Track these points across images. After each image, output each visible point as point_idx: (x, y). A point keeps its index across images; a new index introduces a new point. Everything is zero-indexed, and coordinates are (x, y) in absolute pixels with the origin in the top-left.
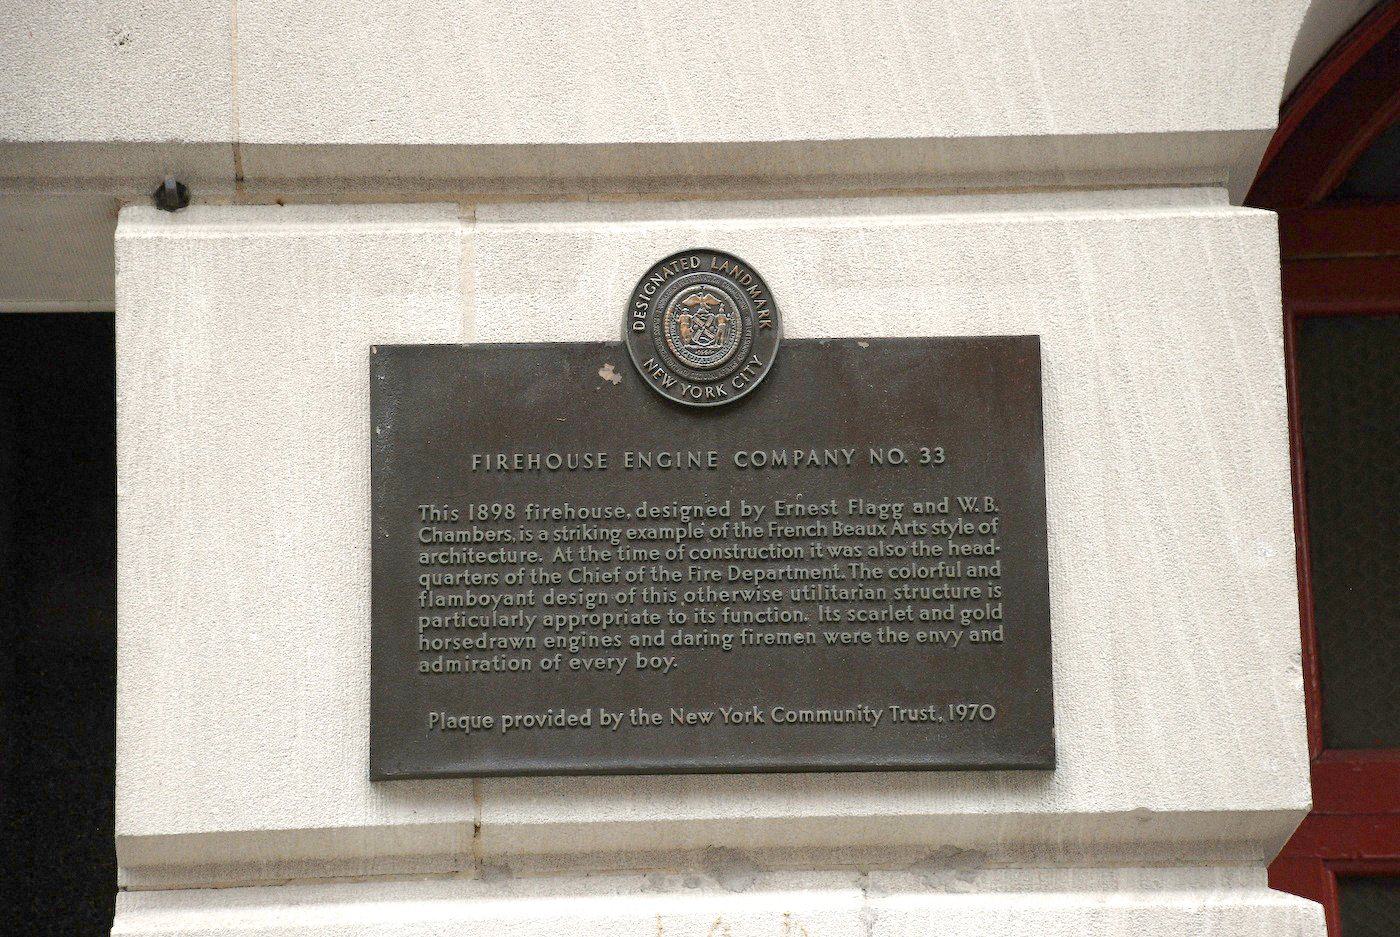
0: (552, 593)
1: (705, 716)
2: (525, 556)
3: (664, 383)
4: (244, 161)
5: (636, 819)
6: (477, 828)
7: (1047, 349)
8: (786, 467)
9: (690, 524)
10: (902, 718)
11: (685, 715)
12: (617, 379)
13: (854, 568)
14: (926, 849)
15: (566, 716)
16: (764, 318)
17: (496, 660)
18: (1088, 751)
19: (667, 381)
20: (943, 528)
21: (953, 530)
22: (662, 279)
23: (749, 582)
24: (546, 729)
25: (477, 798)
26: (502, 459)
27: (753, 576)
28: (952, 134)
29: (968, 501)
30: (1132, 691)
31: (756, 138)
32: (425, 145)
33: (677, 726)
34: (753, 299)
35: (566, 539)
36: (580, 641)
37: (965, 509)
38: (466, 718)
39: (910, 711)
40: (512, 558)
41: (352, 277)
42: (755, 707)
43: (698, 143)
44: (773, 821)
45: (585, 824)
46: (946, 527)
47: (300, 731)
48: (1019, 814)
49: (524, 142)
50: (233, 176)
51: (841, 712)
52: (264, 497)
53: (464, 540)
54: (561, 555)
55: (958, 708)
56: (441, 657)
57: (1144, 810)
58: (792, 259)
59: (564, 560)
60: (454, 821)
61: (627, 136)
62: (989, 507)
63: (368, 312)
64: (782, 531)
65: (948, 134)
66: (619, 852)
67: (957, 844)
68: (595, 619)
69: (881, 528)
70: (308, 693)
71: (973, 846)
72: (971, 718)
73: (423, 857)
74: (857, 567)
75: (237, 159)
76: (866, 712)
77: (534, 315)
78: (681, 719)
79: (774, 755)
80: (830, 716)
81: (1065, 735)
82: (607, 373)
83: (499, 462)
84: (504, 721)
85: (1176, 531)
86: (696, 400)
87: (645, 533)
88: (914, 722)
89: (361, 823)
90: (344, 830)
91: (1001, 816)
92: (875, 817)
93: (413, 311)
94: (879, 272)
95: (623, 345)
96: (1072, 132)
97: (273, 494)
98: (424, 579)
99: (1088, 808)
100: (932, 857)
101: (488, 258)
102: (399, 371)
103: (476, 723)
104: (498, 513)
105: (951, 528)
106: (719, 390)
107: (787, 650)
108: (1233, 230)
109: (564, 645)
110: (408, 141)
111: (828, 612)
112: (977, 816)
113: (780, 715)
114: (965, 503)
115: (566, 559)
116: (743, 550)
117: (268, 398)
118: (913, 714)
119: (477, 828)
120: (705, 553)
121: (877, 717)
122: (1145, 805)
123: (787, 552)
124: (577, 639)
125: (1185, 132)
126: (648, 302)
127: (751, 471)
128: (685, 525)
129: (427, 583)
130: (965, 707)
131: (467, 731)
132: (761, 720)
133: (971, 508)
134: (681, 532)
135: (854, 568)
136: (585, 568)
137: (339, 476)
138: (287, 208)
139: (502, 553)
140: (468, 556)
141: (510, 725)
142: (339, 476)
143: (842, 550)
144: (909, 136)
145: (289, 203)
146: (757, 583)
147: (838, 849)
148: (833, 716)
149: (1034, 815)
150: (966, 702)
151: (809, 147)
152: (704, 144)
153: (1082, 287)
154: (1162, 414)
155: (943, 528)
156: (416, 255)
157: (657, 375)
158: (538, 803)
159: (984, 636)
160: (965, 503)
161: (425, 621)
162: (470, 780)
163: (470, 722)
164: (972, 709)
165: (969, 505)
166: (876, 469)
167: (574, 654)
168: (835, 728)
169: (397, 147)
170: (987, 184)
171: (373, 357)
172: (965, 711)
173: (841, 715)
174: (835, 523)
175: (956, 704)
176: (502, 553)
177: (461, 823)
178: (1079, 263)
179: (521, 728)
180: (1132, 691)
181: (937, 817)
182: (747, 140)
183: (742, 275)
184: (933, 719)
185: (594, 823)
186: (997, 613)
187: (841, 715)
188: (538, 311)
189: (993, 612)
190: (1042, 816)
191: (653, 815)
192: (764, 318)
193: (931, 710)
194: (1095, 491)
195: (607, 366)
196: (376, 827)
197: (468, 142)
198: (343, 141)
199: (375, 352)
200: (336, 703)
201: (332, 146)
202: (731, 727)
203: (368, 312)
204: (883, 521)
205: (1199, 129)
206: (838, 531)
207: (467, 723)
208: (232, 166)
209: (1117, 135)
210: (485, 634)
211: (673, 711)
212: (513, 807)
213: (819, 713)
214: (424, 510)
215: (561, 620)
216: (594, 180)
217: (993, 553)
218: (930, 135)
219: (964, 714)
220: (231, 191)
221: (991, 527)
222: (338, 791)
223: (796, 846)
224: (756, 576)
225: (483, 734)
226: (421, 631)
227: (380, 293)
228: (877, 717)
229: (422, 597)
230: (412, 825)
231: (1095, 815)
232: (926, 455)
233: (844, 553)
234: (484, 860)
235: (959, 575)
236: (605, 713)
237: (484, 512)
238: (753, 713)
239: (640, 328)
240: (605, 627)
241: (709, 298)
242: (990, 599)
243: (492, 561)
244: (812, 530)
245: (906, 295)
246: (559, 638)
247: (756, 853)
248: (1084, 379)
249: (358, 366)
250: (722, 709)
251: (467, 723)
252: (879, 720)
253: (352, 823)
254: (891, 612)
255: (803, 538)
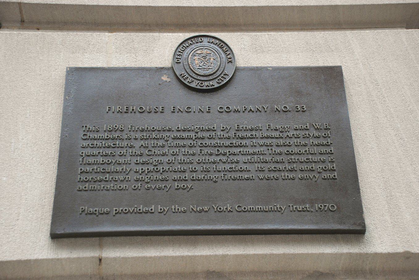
0: (139, 159)
1: (206, 209)
2: (127, 144)
3: (188, 80)
4: (24, 12)
5: (174, 255)
6: (100, 260)
7: (343, 68)
8: (239, 112)
9: (199, 133)
10: (295, 209)
11: (197, 208)
12: (169, 80)
13: (270, 149)
14: (307, 273)
15: (143, 208)
16: (229, 58)
17: (112, 185)
18: (379, 226)
19: (190, 79)
20: (307, 134)
21: (312, 136)
22: (187, 45)
23: (225, 154)
24: (133, 214)
25: (101, 246)
26: (119, 108)
27: (226, 153)
28: (300, 5)
29: (317, 125)
30: (396, 202)
31: (225, 5)
32: (96, 5)
33: (193, 213)
34: (225, 52)
35: (146, 138)
36: (150, 177)
37: (316, 127)
38: (97, 209)
39: (298, 207)
40: (122, 145)
41: (62, 47)
42: (228, 205)
43: (202, 7)
44: (237, 256)
45: (151, 258)
46: (309, 134)
47: (21, 217)
48: (350, 253)
49: (135, 5)
50: (20, 20)
51: (267, 207)
52: (16, 124)
53: (101, 138)
54: (143, 144)
55: (319, 206)
56: (87, 184)
57: (408, 252)
58: (240, 44)
59: (144, 146)
60: (90, 256)
61: (174, 4)
62: (326, 127)
63: (68, 59)
64: (238, 135)
65: (298, 4)
66: (166, 274)
67: (321, 270)
68: (157, 169)
69: (281, 135)
70: (26, 202)
71: (328, 271)
72: (326, 209)
73: (75, 276)
74: (271, 149)
75: (21, 12)
76: (278, 207)
77: (136, 61)
78: (195, 210)
79: (238, 225)
80: (262, 208)
81: (369, 221)
82: (165, 78)
83: (118, 109)
84: (114, 210)
85: (406, 139)
86: (202, 86)
87: (180, 136)
88: (300, 211)
89: (45, 257)
90: (36, 261)
91: (342, 254)
92: (284, 254)
93: (87, 59)
94: (275, 48)
95: (172, 68)
96: (346, 4)
97: (20, 123)
98: (82, 153)
99: (382, 251)
100: (309, 276)
101: (119, 42)
102: (76, 74)
103: (101, 211)
104: (117, 128)
105: (311, 134)
106: (211, 83)
107: (242, 182)
108: (414, 34)
109: (143, 179)
110: (89, 4)
111: (259, 166)
112: (331, 254)
113: (239, 208)
114: (316, 125)
115: (145, 145)
116: (222, 143)
117: (22, 88)
118: (300, 208)
119: (100, 260)
120: (206, 144)
121: (283, 209)
122: (408, 250)
123: (241, 143)
124: (149, 177)
125: (390, 4)
126: (182, 53)
127: (224, 113)
128: (197, 133)
129: (84, 154)
130: (322, 205)
131: (97, 214)
132: (231, 210)
133: (319, 127)
134: (195, 136)
135: (270, 149)
136: (153, 149)
137: (49, 117)
138: (40, 30)
139: (117, 143)
140: (102, 144)
141: (117, 212)
142: (49, 117)
143: (265, 143)
144: (283, 5)
145: (41, 29)
146: (228, 155)
147: (266, 272)
148: (263, 209)
149: (357, 254)
150: (323, 203)
151: (245, 9)
152: (205, 7)
153: (356, 53)
154: (394, 96)
155: (307, 134)
156: (89, 40)
157: (185, 78)
158: (129, 248)
159: (328, 176)
160: (316, 125)
161: (81, 169)
162: (98, 238)
163: (99, 211)
164: (326, 206)
165: (317, 126)
166: (277, 112)
167: (147, 183)
168: (265, 213)
169: (84, 6)
170: (313, 27)
171: (67, 71)
172: (323, 206)
173: (267, 208)
174: (261, 132)
175: (318, 204)
176: (117, 143)
177: (93, 257)
178: (354, 45)
179: (122, 213)
180: (396, 202)
181: (312, 254)
182: (221, 6)
183: (220, 44)
184: (308, 210)
185: (155, 256)
186: (333, 167)
187: (267, 208)
188: (137, 60)
189: (332, 167)
190: (361, 254)
191: (182, 253)
192: (229, 58)
193: (307, 206)
194: (369, 124)
195: (165, 76)
196: (52, 260)
197: (112, 4)
198: (63, 3)
199: (68, 69)
200: (39, 206)
201: (58, 5)
202: (218, 213)
203: (68, 59)
204: (281, 132)
205: (396, 3)
206: (262, 136)
207: (97, 211)
208: (19, 15)
209: (364, 5)
210: (108, 175)
211: (191, 207)
212: (117, 250)
213: (257, 207)
214: (84, 127)
215: (142, 169)
216: (162, 25)
217: (329, 144)
218: (292, 5)
219: (322, 208)
220: (19, 25)
221: (328, 134)
222: (36, 243)
223: (247, 271)
224: (228, 152)
225: (105, 216)
226: (79, 173)
227: (73, 53)
228: (283, 209)
229: (81, 160)
230: (69, 258)
231: (385, 254)
232: (298, 107)
233: (266, 144)
234: (104, 277)
235: (316, 153)
236: (160, 207)
237: (111, 128)
238: (227, 207)
239: (178, 61)
240: (161, 172)
241: (207, 51)
242: (330, 162)
243: (113, 146)
244: (251, 135)
245: (286, 56)
246: (141, 176)
247: (229, 274)
248: (360, 85)
249: (62, 78)
250: (214, 206)
251: (97, 211)
252: (284, 210)
253: (40, 257)
254: (287, 167)
255: (248, 138)
